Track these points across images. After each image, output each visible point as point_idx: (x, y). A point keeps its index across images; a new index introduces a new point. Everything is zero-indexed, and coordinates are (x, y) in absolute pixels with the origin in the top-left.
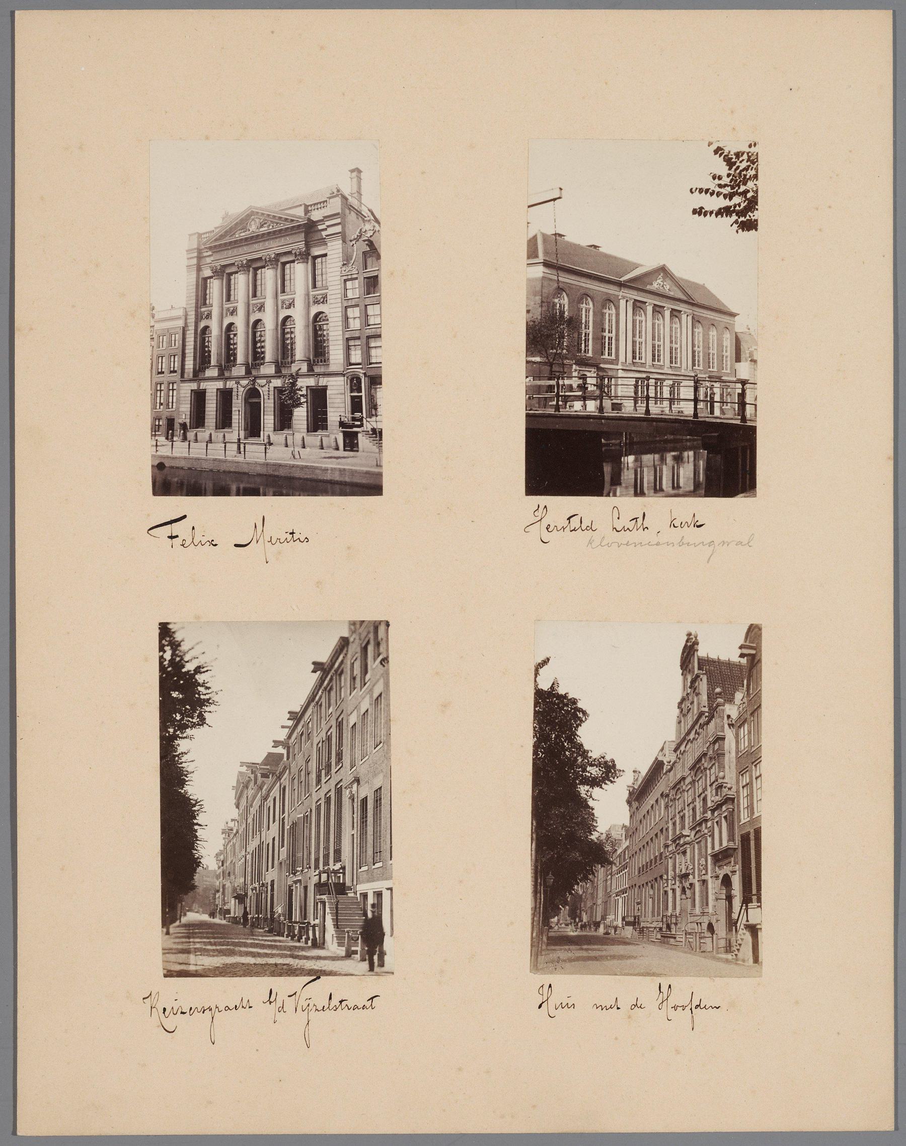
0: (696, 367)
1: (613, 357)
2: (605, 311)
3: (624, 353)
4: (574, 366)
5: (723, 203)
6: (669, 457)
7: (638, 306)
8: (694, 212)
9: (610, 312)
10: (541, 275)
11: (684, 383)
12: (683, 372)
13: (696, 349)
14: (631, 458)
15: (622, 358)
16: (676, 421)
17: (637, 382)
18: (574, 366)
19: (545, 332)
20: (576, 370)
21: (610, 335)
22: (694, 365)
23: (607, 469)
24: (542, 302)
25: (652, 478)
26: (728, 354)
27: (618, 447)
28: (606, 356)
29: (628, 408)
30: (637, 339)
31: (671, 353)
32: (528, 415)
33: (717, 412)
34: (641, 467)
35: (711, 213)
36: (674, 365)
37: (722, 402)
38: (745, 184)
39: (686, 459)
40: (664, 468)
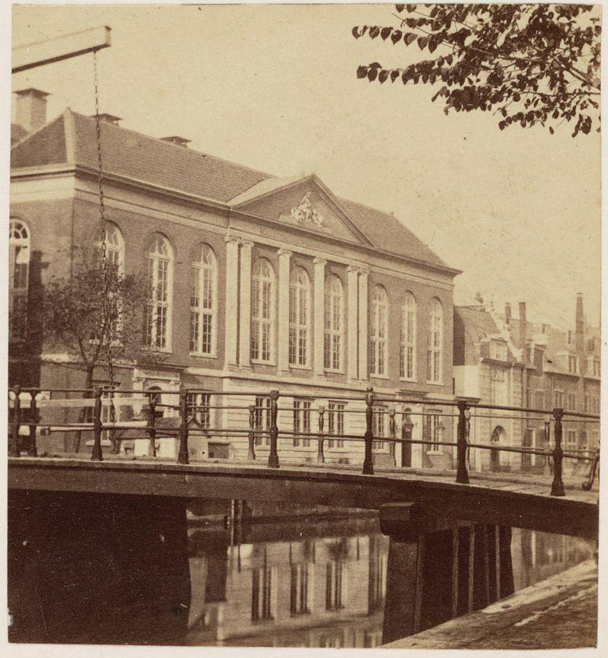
0: (376, 375)
1: (213, 353)
2: (197, 264)
3: (235, 343)
4: (136, 372)
5: (416, 55)
6: (321, 547)
7: (262, 255)
8: (362, 72)
9: (207, 268)
10: (71, 194)
11: (351, 405)
12: (349, 384)
13: (376, 338)
14: (246, 550)
15: (230, 356)
16: (330, 478)
17: (259, 402)
18: (136, 372)
19: (78, 304)
20: (139, 380)
21: (381, 339)
22: (371, 369)
23: (198, 569)
24: (74, 247)
25: (287, 587)
26: (440, 348)
27: (220, 528)
28: (199, 352)
29: (240, 456)
30: (260, 318)
31: (327, 346)
32: (12, 466)
33: (416, 462)
34: (265, 567)
35: (395, 74)
36: (331, 369)
37: (427, 442)
38: (461, 19)
39: (353, 552)
40: (311, 569)
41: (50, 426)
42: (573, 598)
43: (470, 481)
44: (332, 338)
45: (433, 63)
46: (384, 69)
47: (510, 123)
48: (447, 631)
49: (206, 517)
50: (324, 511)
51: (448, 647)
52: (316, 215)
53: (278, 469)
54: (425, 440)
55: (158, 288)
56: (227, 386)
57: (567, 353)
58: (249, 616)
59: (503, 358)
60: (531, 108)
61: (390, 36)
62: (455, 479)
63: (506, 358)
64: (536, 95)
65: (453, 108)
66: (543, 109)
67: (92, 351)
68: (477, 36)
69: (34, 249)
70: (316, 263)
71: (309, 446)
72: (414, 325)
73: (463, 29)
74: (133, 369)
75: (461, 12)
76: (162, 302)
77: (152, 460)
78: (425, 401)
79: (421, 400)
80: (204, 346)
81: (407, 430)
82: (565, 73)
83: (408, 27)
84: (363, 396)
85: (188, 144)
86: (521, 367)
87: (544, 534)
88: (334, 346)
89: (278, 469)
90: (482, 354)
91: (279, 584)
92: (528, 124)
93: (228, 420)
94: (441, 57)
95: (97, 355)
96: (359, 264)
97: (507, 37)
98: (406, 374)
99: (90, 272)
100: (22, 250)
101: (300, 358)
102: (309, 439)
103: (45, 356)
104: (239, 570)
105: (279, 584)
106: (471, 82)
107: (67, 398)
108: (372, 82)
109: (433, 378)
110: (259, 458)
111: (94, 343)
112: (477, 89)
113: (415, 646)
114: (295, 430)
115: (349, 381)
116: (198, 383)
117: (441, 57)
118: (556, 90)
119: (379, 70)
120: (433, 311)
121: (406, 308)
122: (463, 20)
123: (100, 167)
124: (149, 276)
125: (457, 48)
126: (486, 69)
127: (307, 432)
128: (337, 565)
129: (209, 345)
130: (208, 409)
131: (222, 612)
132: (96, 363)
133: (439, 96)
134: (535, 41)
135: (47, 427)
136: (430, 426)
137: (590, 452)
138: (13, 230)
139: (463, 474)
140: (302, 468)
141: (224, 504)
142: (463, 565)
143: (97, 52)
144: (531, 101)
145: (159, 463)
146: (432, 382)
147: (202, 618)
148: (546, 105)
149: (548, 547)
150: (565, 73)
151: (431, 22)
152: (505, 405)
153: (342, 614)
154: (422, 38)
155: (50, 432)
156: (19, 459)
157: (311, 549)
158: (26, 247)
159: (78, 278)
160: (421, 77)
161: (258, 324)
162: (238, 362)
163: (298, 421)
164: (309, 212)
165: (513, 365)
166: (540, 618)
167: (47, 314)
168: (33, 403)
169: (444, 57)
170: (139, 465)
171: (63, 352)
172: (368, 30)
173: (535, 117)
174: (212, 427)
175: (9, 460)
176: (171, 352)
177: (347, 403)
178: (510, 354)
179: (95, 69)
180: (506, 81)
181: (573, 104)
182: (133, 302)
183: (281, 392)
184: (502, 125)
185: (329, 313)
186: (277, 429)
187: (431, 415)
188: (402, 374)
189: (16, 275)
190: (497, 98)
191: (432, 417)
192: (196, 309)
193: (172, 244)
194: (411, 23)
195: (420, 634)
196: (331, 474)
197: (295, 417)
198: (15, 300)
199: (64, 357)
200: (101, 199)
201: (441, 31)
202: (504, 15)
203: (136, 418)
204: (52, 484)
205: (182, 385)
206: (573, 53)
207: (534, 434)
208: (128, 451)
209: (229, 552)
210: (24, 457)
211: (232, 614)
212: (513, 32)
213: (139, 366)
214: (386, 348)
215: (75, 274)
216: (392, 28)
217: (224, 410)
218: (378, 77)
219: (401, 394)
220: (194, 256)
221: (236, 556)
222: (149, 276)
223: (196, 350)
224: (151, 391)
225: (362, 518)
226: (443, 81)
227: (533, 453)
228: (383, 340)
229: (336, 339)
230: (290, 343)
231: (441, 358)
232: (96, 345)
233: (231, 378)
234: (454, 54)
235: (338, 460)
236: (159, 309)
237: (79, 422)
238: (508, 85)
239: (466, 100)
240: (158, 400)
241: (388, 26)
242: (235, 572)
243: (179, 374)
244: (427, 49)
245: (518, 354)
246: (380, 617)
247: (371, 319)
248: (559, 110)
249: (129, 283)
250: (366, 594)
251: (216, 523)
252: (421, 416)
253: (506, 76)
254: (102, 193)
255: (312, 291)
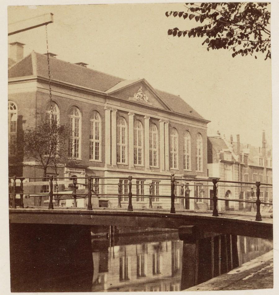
0: (173, 168)
1: (100, 160)
2: (92, 120)
3: (109, 156)
5: (195, 24)
6: (150, 246)
7: (121, 115)
8: (170, 32)
9: (97, 121)
10: (36, 89)
12: (161, 172)
13: (173, 152)
14: (117, 248)
15: (107, 161)
16: (156, 215)
17: (121, 181)
18: (66, 169)
20: (67, 172)
22: (171, 166)
23: (96, 258)
24: (37, 113)
26: (201, 156)
27: (105, 239)
29: (114, 205)
30: (121, 144)
31: (151, 156)
32: (11, 212)
33: (192, 207)
34: (125, 256)
35: (185, 33)
36: (153, 166)
39: (164, 248)
41: (29, 194)
42: (268, 267)
43: (219, 215)
44: (153, 152)
45: (202, 28)
46: (180, 31)
47: (237, 54)
48: (213, 283)
49: (98, 234)
50: (151, 230)
51: (213, 290)
52: (145, 97)
53: (133, 212)
54: (196, 197)
55: (75, 130)
56: (107, 175)
57: (259, 157)
58: (118, 278)
59: (230, 160)
60: (246, 47)
61: (183, 16)
62: (212, 214)
63: (231, 159)
64: (248, 42)
65: (211, 48)
66: (252, 48)
67: (46, 160)
68: (222, 15)
69: (19, 115)
70: (160, 122)
71: (143, 201)
72: (190, 146)
73: (215, 12)
74: (64, 168)
75: (214, 5)
76: (77, 137)
77: (75, 209)
78: (196, 179)
79: (193, 179)
80: (96, 157)
81: (188, 193)
82: (262, 31)
83: (191, 12)
84: (170, 178)
85: (87, 66)
86: (238, 164)
87: (250, 238)
88: (154, 155)
89: (133, 212)
90: (220, 158)
91: (132, 265)
92: (245, 55)
93: (107, 190)
94: (206, 25)
95: (48, 162)
96: (164, 119)
97: (235, 16)
98: (186, 167)
99: (45, 124)
100: (14, 115)
101: (139, 161)
102: (144, 198)
103: (25, 163)
104: (114, 257)
105: (132, 265)
106: (219, 36)
107: (35, 181)
108: (175, 37)
109: (198, 169)
110: (123, 207)
111: (47, 156)
112: (222, 39)
113: (199, 290)
114: (137, 194)
115: (161, 171)
116: (94, 173)
117: (206, 25)
118: (257, 39)
119: (178, 31)
120: (198, 139)
121: (186, 138)
122: (216, 8)
123: (50, 77)
124: (71, 126)
125: (213, 21)
126: (226, 30)
127: (142, 195)
128: (157, 255)
129: (98, 156)
130: (98, 185)
131: (106, 276)
132: (48, 165)
133: (205, 43)
134: (248, 17)
135: (28, 195)
136: (198, 191)
137: (270, 201)
138: (10, 106)
139: (215, 212)
140: (143, 211)
141: (106, 228)
142: (216, 253)
143: (47, 25)
144: (246, 44)
145: (79, 210)
146: (198, 171)
147: (98, 279)
148: (253, 46)
149: (252, 244)
150: (262, 31)
151: (201, 9)
152: (231, 180)
153: (160, 276)
154: (197, 16)
155: (29, 197)
156: (16, 209)
157: (146, 247)
158: (16, 114)
159: (39, 127)
160: (197, 34)
161: (120, 146)
162: (111, 164)
163: (139, 190)
164: (142, 95)
165: (234, 163)
166: (254, 276)
167: (26, 144)
168: (22, 184)
169: (207, 25)
170: (44, 210)
171: (33, 161)
172: (173, 13)
173: (248, 52)
174: (100, 193)
175: (9, 210)
176: (81, 160)
177: (160, 181)
178: (233, 158)
179: (46, 30)
180: (235, 35)
181: (265, 45)
182: (64, 137)
183: (133, 177)
184: (234, 55)
185: (152, 141)
186: (132, 194)
187: (198, 186)
188: (185, 168)
189: (11, 126)
190: (231, 43)
191: (199, 187)
192: (92, 140)
193: (81, 112)
194: (192, 10)
195: (200, 285)
196: (156, 213)
197: (137, 188)
198: (11, 137)
199: (33, 163)
200: (50, 92)
201: (206, 13)
202: (233, 6)
203: (66, 190)
204: (28, 220)
205: (86, 174)
206: (265, 22)
207: (244, 193)
208: (63, 205)
209: (109, 250)
210: (19, 208)
211: (110, 278)
212: (238, 13)
213: (67, 166)
214: (177, 156)
215: (38, 126)
216: (183, 12)
217: (105, 185)
218: (177, 35)
219: (184, 176)
220: (91, 116)
221: (112, 252)
222: (71, 126)
223: (92, 158)
224: (72, 177)
225: (168, 233)
226: (207, 36)
227: (244, 202)
228: (176, 152)
229: (155, 153)
230: (134, 155)
231: (202, 160)
232: (48, 157)
233: (108, 171)
234: (212, 23)
235: (156, 207)
236: (75, 140)
237: (41, 192)
238: (236, 37)
239: (218, 44)
240: (76, 181)
241: (182, 11)
242: (112, 259)
243: (85, 170)
244: (199, 21)
245: (237, 158)
246: (179, 277)
247: (170, 143)
248: (259, 48)
249: (62, 129)
250: (170, 268)
251: (103, 237)
252: (194, 186)
253: (235, 33)
254: (50, 89)
255: (144, 131)
